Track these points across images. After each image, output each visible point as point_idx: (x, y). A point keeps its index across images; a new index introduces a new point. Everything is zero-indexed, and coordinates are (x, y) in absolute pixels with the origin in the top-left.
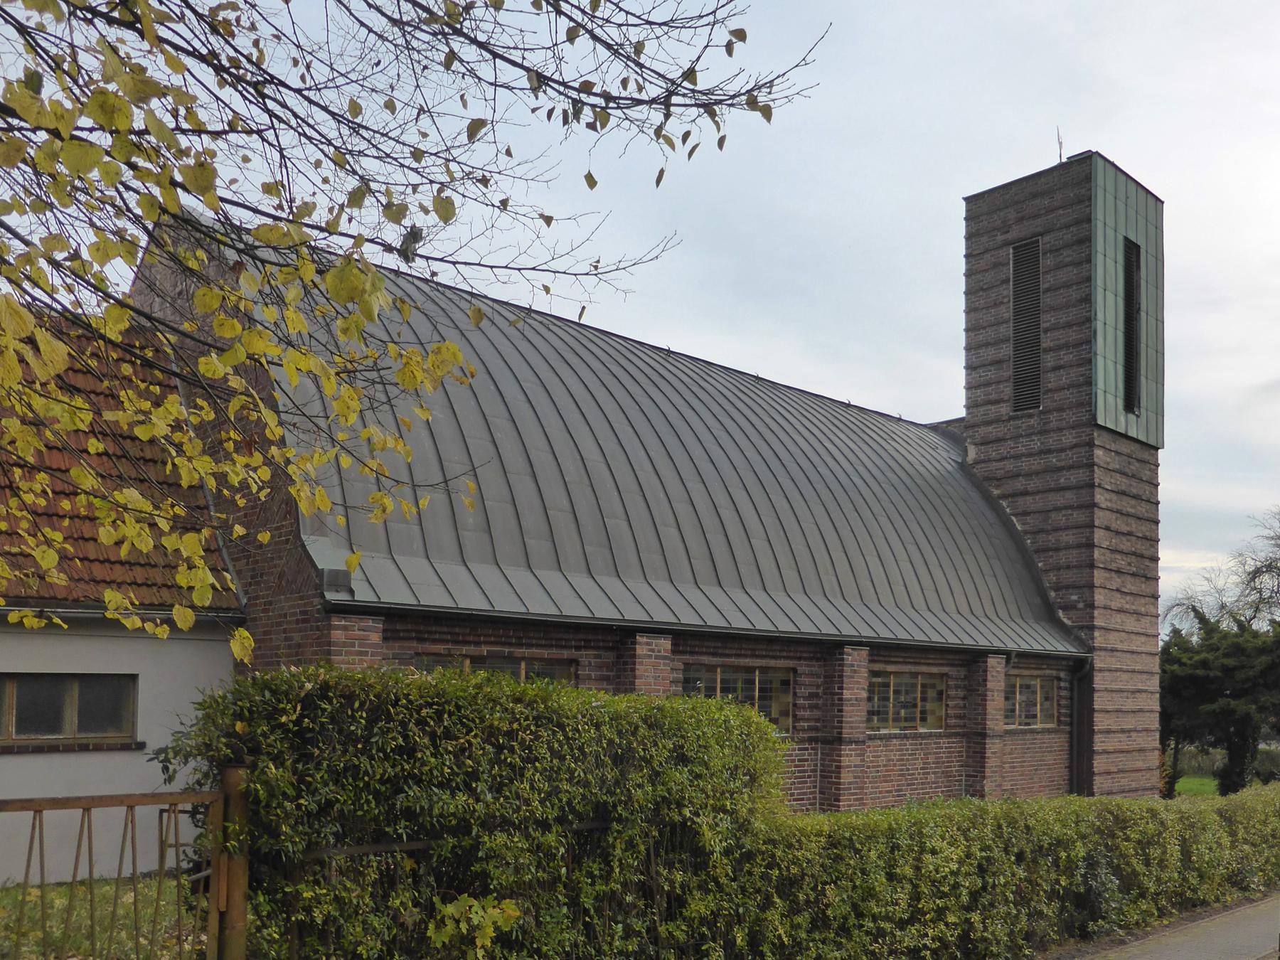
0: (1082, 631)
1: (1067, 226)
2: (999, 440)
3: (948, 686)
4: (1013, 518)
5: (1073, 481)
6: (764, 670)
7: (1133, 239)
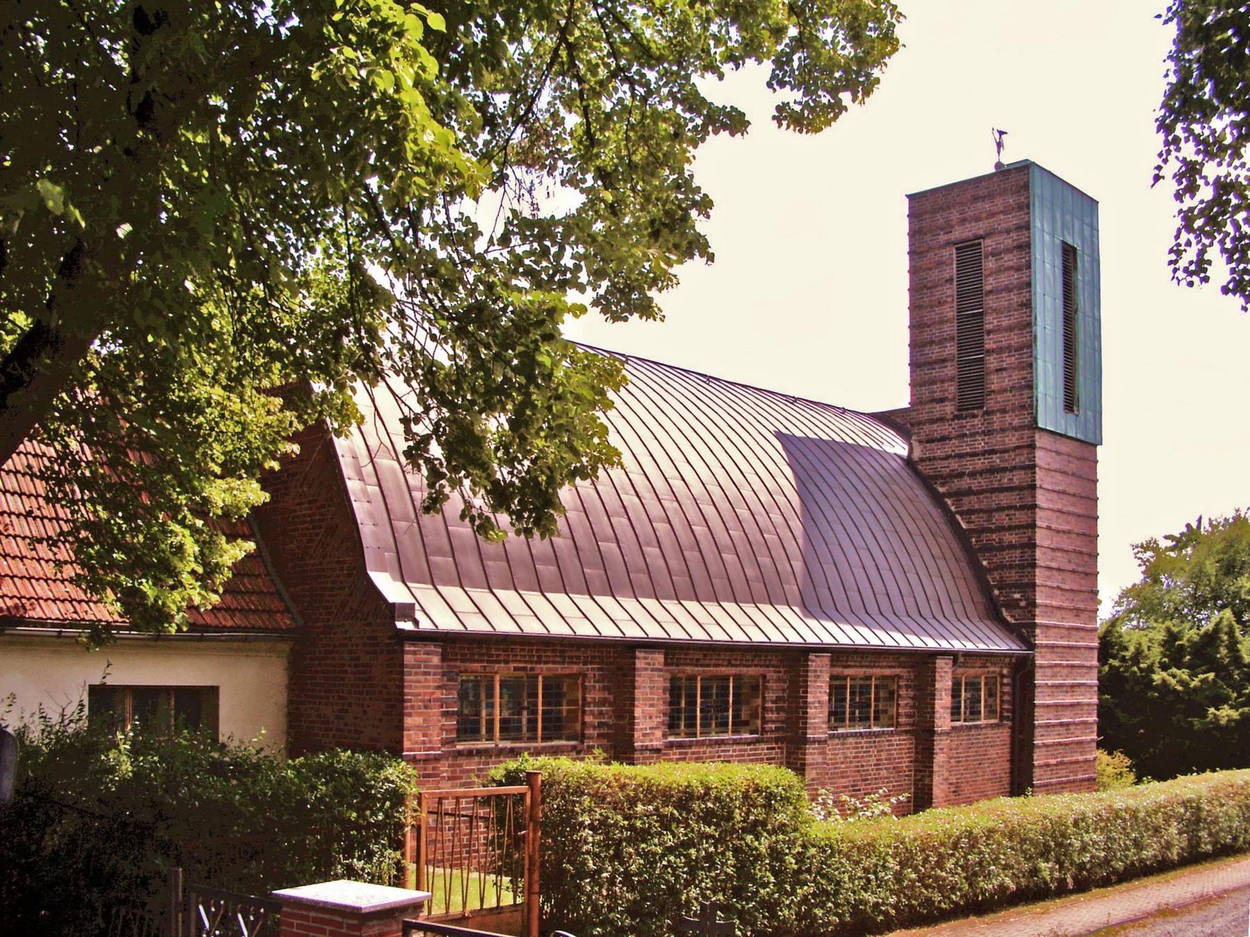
0: (1024, 632)
1: (1008, 231)
2: (943, 439)
3: (899, 687)
4: (958, 517)
5: (1016, 482)
6: (738, 678)
7: (1070, 242)
